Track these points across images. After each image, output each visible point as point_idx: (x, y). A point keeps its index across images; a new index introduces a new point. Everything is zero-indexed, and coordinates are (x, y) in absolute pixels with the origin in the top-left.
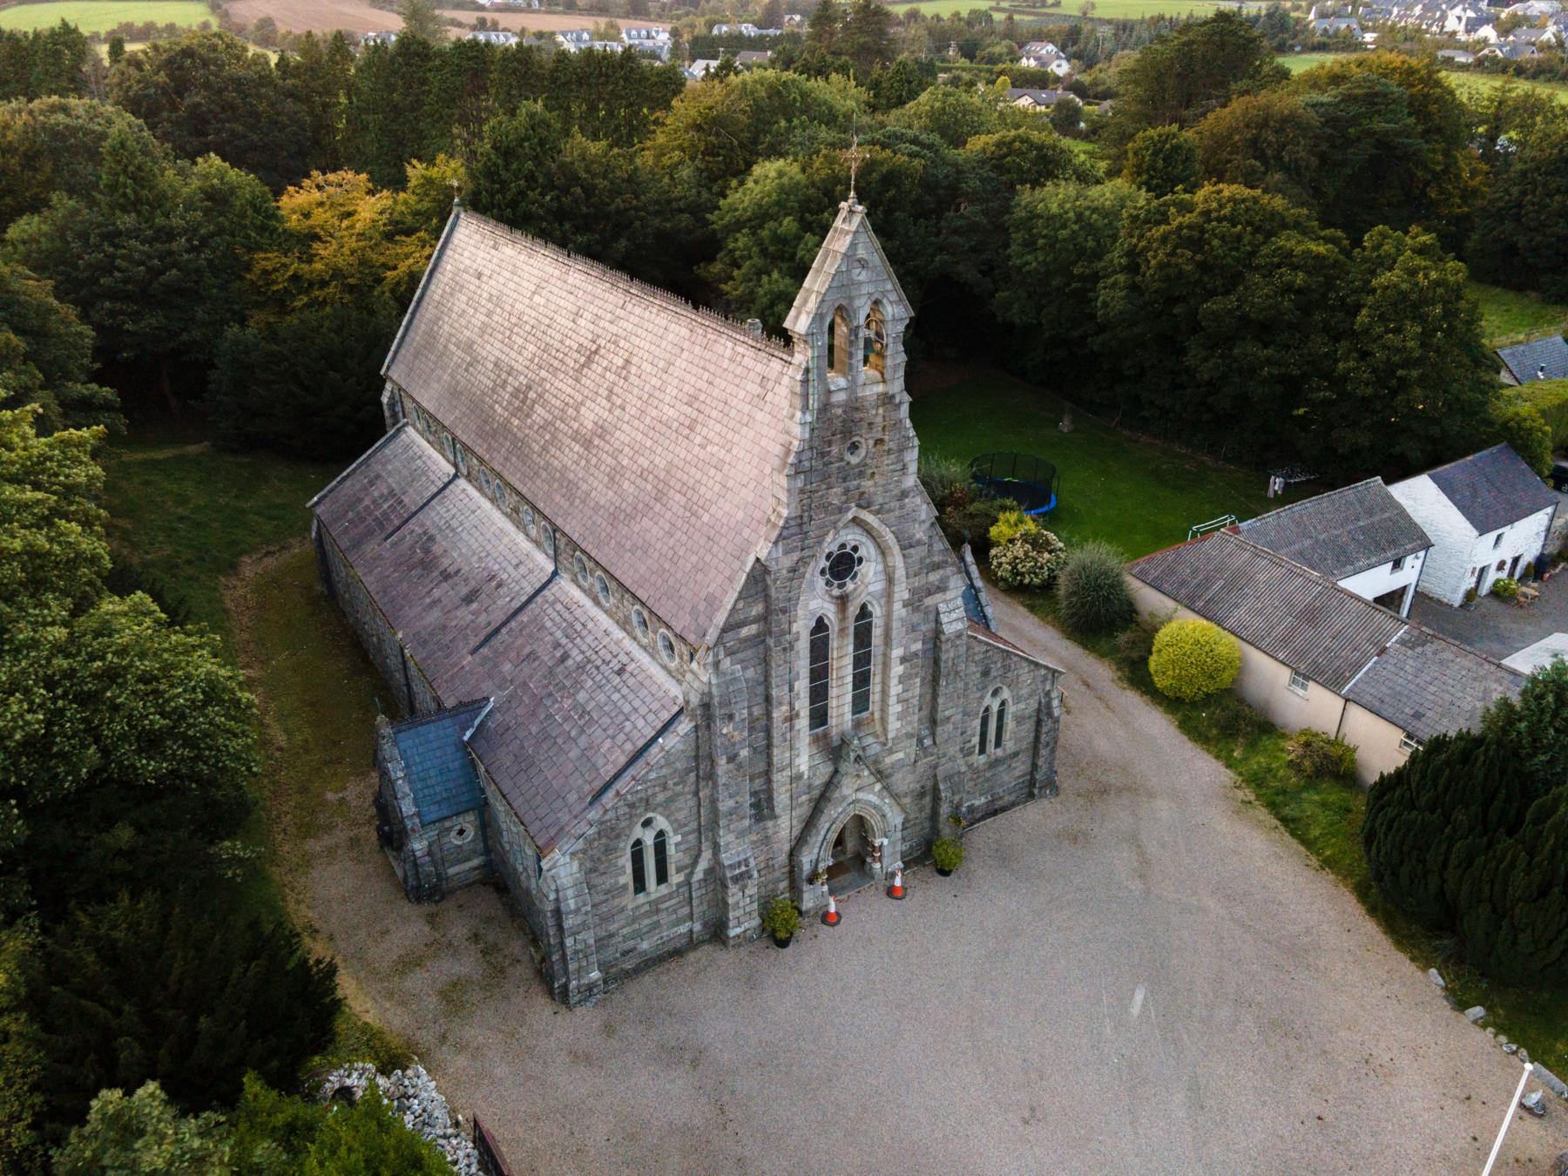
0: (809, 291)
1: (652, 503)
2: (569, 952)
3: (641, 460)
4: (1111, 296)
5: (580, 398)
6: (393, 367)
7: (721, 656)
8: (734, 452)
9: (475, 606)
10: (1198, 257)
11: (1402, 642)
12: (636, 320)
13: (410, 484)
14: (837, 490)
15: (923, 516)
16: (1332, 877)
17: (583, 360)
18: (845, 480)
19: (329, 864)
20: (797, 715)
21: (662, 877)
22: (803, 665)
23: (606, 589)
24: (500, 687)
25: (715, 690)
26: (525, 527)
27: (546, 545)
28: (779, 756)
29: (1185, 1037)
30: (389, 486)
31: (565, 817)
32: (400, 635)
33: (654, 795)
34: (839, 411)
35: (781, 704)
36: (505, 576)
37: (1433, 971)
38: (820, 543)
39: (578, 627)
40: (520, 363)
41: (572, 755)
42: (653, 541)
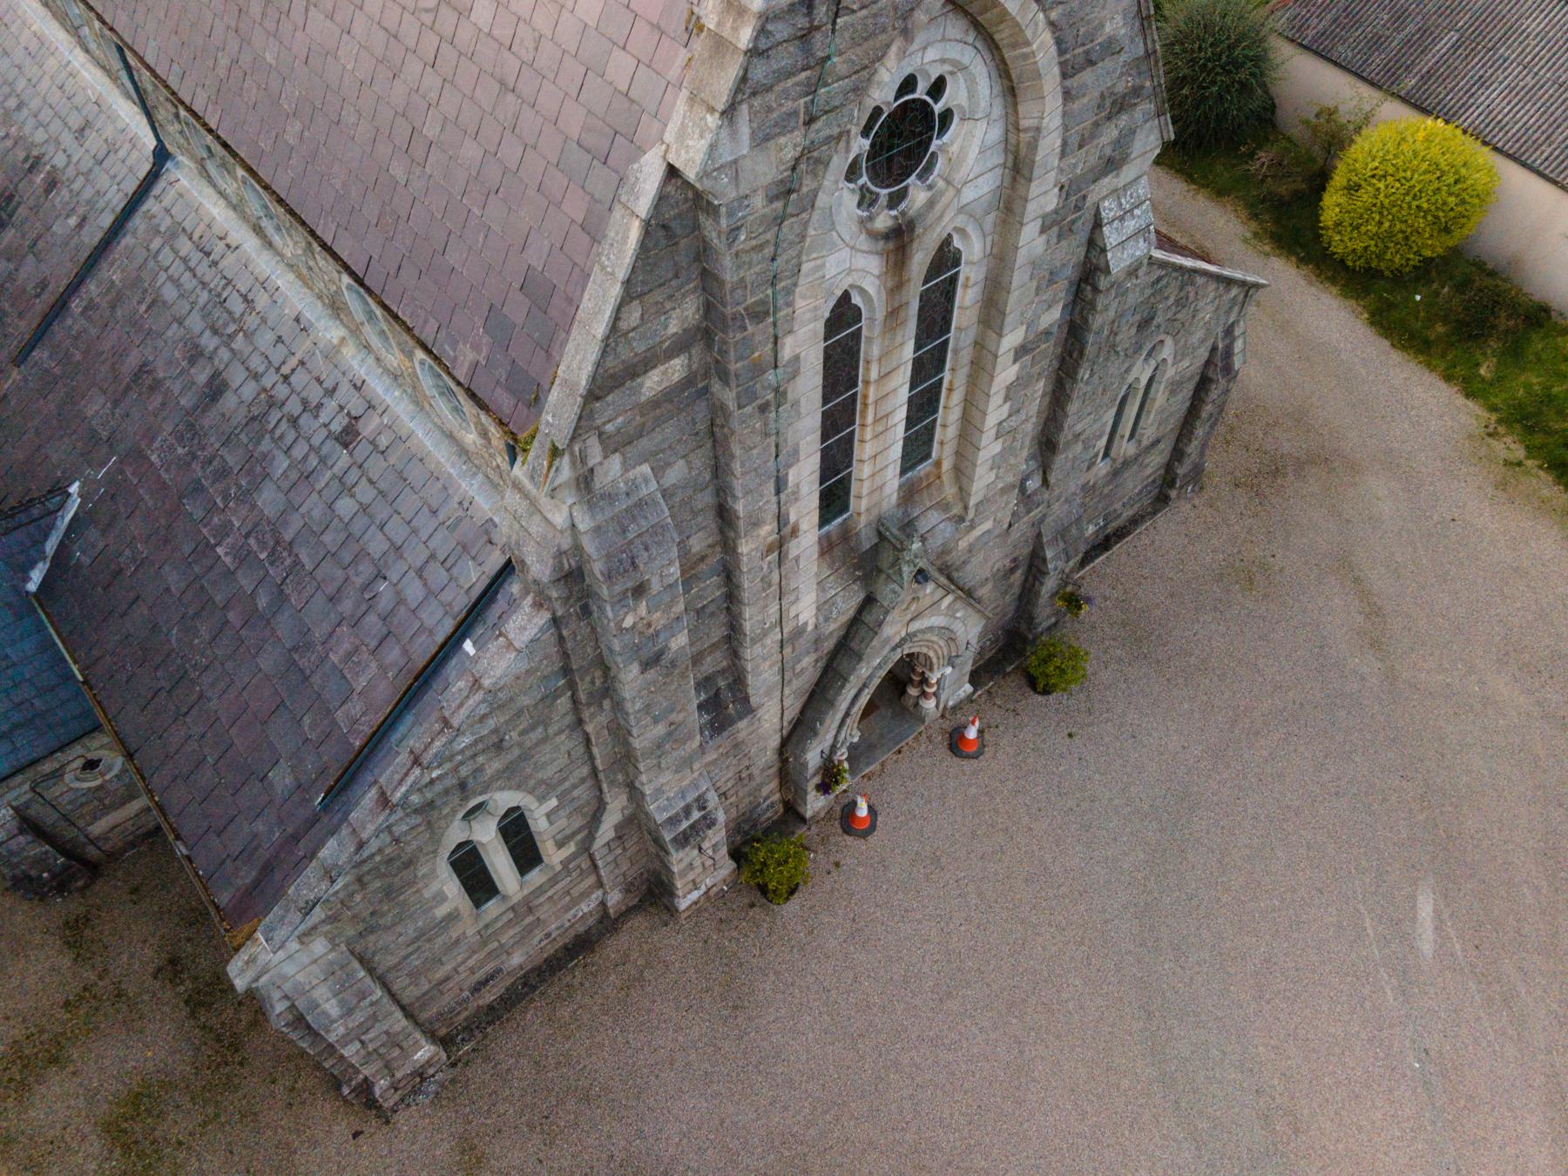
25: (589, 546)
35: (756, 524)
36: (60, 160)
39: (237, 306)
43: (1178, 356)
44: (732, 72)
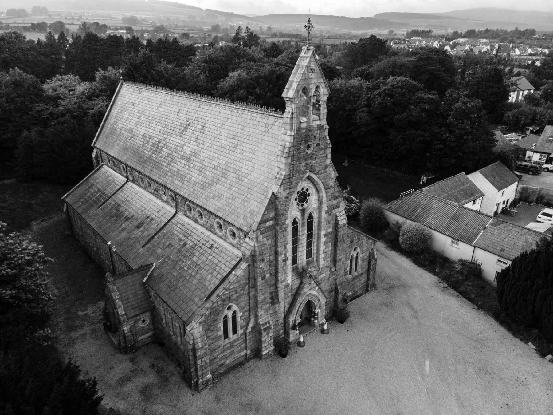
0: (292, 82)
1: (220, 178)
2: (199, 367)
3: (213, 163)
4: (362, 116)
5: (183, 143)
6: (97, 143)
7: (259, 235)
8: (256, 153)
9: (142, 229)
10: (392, 100)
11: (492, 224)
12: (206, 111)
13: (107, 186)
14: (303, 164)
15: (333, 176)
16: (483, 312)
17: (183, 128)
18: (306, 160)
19: (83, 341)
20: (288, 259)
21: (235, 332)
22: (290, 238)
23: (201, 215)
24: (157, 259)
25: (257, 249)
26: (161, 196)
27: (171, 202)
28: (281, 276)
29: (449, 378)
30: (98, 188)
31: (194, 308)
32: (109, 243)
33: (232, 295)
34: (304, 131)
35: (281, 254)
36: (154, 216)
37: (530, 343)
38: (296, 186)
40: (154, 133)
41: (194, 282)
42: (222, 193)
43: (363, 252)
44: (281, 181)
